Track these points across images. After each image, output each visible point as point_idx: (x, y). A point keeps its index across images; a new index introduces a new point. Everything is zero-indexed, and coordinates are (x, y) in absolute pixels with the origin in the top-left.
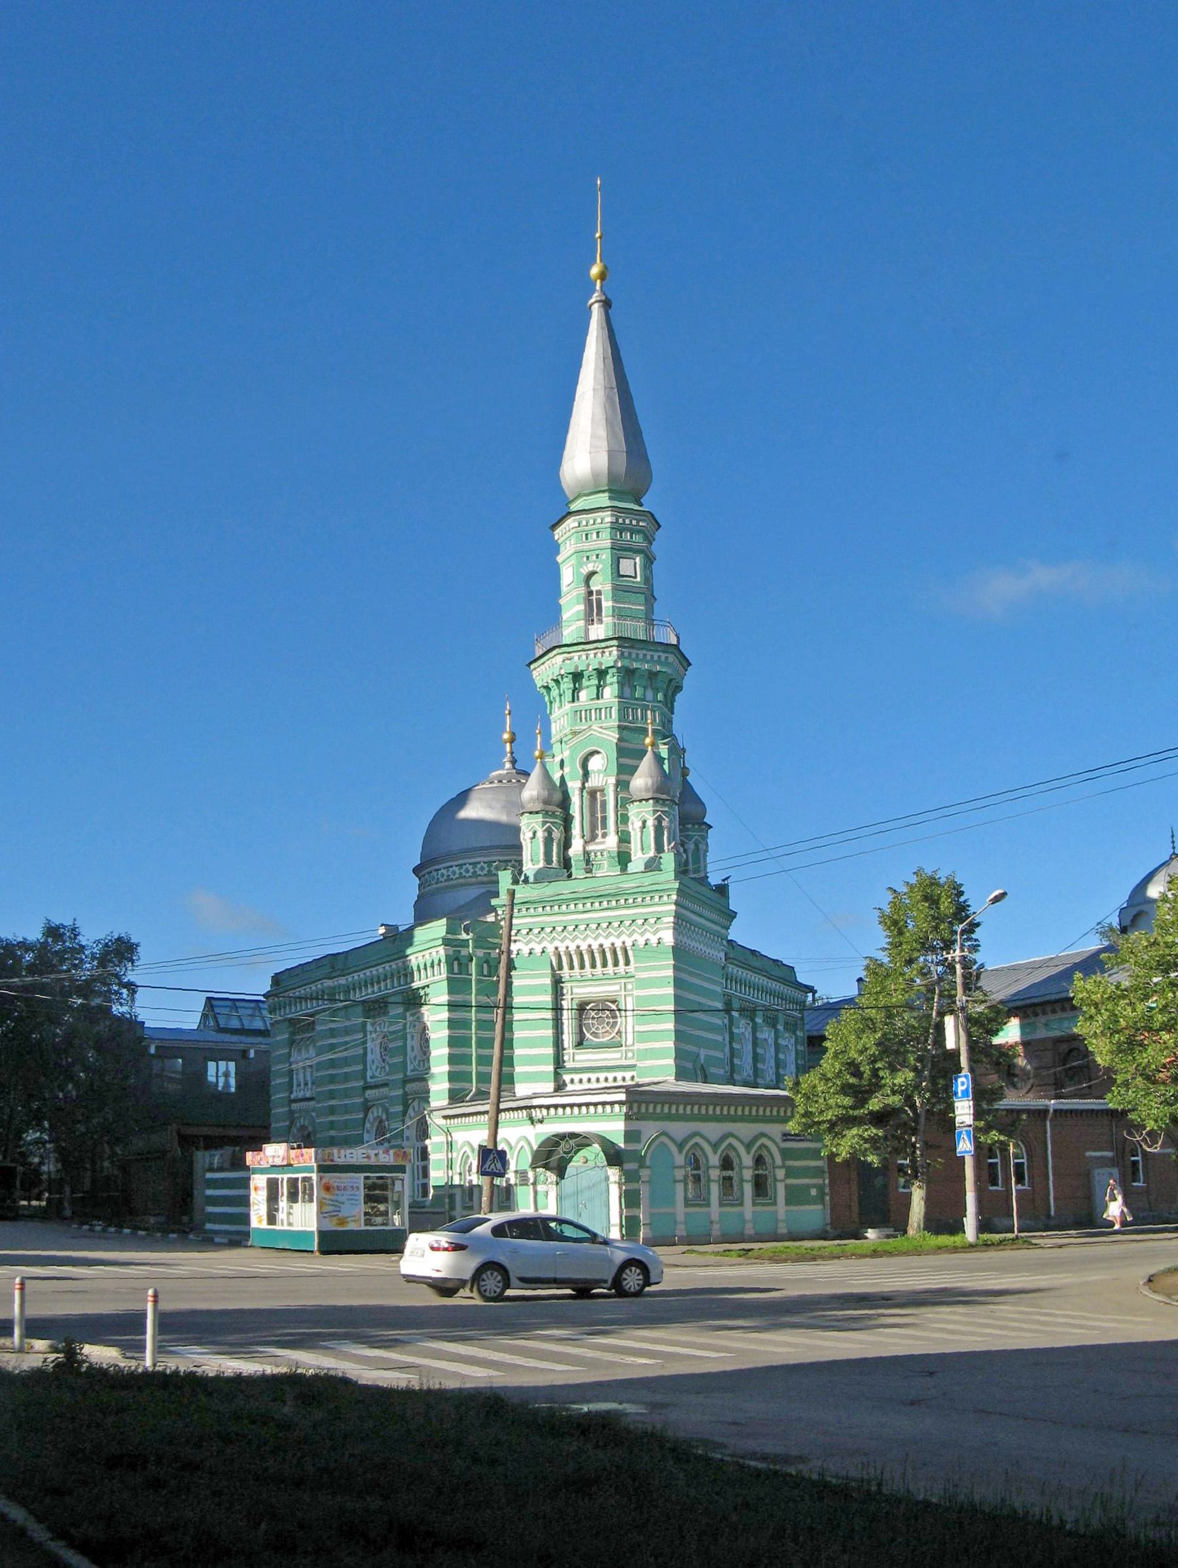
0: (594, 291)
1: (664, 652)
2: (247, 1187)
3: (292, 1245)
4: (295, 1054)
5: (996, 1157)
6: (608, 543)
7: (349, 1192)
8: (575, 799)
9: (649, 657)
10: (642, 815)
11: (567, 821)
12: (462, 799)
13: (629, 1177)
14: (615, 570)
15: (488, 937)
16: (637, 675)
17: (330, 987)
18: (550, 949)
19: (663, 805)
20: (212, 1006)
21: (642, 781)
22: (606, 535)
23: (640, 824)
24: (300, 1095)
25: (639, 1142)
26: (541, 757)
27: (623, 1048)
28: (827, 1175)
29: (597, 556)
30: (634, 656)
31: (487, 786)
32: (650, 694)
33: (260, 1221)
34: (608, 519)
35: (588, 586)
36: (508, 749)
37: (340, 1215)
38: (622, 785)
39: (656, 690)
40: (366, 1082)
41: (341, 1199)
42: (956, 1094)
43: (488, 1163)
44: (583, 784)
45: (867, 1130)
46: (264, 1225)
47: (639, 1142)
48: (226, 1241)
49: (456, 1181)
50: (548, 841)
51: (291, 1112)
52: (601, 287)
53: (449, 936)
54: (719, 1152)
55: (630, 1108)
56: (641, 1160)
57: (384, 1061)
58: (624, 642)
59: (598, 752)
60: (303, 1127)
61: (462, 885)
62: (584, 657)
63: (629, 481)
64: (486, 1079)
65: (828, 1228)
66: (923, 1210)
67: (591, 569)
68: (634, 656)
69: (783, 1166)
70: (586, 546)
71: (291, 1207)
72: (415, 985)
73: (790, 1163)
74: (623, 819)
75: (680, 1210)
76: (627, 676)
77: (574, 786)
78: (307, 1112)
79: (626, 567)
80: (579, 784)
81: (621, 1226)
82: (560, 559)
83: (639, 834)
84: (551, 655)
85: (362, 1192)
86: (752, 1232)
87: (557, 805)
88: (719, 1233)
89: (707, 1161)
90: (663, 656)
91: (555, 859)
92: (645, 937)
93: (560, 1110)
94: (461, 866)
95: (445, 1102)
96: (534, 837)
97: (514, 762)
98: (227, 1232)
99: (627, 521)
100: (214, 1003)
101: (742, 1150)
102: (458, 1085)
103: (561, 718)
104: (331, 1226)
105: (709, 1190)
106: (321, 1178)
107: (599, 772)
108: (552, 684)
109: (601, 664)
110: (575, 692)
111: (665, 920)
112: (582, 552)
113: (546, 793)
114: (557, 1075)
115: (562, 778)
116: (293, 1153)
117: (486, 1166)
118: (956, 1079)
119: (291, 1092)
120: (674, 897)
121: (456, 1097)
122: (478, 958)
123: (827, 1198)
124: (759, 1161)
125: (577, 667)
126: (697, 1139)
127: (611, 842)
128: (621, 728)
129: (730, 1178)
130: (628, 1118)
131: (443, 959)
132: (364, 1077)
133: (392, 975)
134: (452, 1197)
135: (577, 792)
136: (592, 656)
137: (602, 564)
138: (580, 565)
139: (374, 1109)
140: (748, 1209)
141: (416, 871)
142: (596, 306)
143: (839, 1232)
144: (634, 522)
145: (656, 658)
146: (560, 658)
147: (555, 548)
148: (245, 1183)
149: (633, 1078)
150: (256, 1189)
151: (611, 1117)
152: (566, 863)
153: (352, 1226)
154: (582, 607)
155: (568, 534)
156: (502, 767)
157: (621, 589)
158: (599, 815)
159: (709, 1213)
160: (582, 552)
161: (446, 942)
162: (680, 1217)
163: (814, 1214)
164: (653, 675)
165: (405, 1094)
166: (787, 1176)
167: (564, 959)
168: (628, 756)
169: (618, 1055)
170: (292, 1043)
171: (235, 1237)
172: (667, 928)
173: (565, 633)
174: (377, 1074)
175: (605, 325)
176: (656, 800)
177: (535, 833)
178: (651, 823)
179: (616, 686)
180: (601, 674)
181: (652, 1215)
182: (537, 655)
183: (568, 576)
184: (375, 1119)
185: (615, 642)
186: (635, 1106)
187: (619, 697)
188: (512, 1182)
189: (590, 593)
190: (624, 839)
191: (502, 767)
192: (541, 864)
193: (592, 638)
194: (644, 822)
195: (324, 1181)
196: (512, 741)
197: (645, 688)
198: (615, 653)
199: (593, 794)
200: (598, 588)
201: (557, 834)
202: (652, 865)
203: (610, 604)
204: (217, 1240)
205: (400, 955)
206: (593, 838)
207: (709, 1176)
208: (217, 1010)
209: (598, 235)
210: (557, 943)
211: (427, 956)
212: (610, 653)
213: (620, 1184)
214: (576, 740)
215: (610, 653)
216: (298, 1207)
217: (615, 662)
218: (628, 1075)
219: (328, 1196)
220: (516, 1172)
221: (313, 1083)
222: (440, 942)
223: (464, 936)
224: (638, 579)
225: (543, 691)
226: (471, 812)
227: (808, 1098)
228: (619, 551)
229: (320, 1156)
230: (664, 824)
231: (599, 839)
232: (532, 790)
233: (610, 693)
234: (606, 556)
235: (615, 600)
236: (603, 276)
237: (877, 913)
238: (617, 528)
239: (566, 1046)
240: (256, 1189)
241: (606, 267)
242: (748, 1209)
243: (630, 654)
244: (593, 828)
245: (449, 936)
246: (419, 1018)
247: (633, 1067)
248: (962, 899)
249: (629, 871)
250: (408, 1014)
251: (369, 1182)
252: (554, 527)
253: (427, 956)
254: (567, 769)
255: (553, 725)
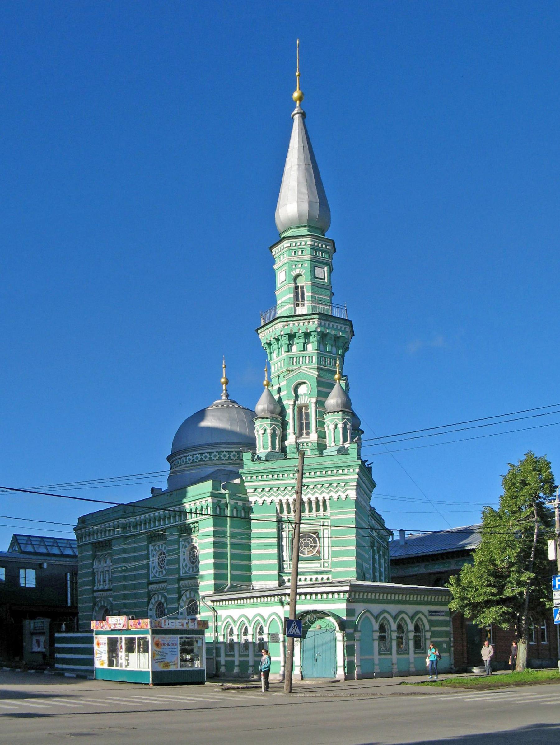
0: (295, 107)
1: (344, 324)
2: (92, 642)
3: (134, 680)
4: (96, 565)
5: (544, 626)
6: (309, 257)
7: (170, 647)
8: (289, 412)
9: (335, 327)
10: (334, 423)
11: (284, 425)
12: (201, 415)
13: (349, 637)
14: (313, 274)
15: (239, 492)
16: (328, 337)
17: (123, 523)
18: (277, 501)
19: (348, 415)
20: (17, 540)
21: (333, 400)
22: (307, 252)
23: (334, 426)
24: (101, 587)
25: (354, 616)
26: (268, 385)
27: (322, 561)
28: (452, 635)
29: (302, 265)
30: (327, 325)
31: (214, 407)
32: (334, 350)
33: (102, 664)
34: (309, 243)
35: (295, 283)
36: (224, 388)
37: (166, 661)
38: (320, 403)
39: (338, 348)
40: (149, 580)
41: (165, 651)
42: (554, 586)
43: (291, 629)
44: (295, 402)
45: (501, 608)
46: (106, 666)
47: (354, 616)
48: (74, 675)
49: (221, 639)
50: (273, 436)
51: (94, 598)
52: (300, 105)
53: (214, 491)
54: (397, 623)
55: (350, 595)
56: (355, 627)
57: (161, 568)
58: (323, 317)
59: (304, 383)
60: (102, 607)
61: (200, 465)
62: (296, 324)
63: (318, 224)
64: (235, 580)
65: (453, 666)
66: (526, 656)
67: (298, 273)
68: (327, 325)
69: (430, 631)
70: (295, 258)
71: (128, 656)
72: (189, 521)
73: (433, 629)
74: (321, 424)
75: (376, 657)
76: (323, 337)
77: (288, 403)
78: (106, 597)
79: (319, 272)
80: (292, 402)
81: (344, 667)
82: (275, 267)
83: (333, 432)
84: (274, 323)
85: (178, 647)
86: (414, 669)
87: (278, 413)
88: (397, 670)
89: (390, 627)
90: (344, 327)
91: (277, 447)
92: (338, 494)
93: (319, 596)
94: (201, 454)
95: (212, 592)
96: (265, 433)
97: (227, 396)
98: (73, 670)
99: (320, 245)
100: (18, 537)
101: (408, 620)
102: (220, 582)
103: (278, 361)
104: (160, 668)
105: (391, 645)
106: (153, 638)
107: (305, 394)
108: (273, 341)
109: (307, 329)
110: (290, 346)
111: (351, 484)
112: (290, 264)
113: (273, 407)
114: (280, 576)
115: (280, 399)
116: (131, 622)
117: (290, 630)
118: (554, 579)
119: (94, 586)
120: (357, 470)
121: (218, 589)
122: (231, 506)
123: (453, 649)
124: (417, 628)
125: (291, 330)
126: (274, 617)
127: (314, 437)
128: (319, 369)
129: (419, 636)
130: (348, 601)
131: (210, 505)
132: (179, 573)
133: (150, 520)
134: (218, 649)
135: (291, 407)
136: (301, 324)
137: (305, 270)
138: (291, 270)
139: (156, 596)
140: (394, 656)
141: (169, 459)
142: (297, 116)
143: (457, 669)
144: (324, 246)
145: (339, 328)
146: (280, 325)
147: (273, 261)
148: (90, 640)
149: (328, 579)
150: (98, 644)
151: (338, 600)
152: (283, 450)
153: (172, 668)
154: (292, 295)
155: (282, 251)
156: (220, 398)
157: (316, 285)
158: (304, 421)
159: (391, 659)
160: (290, 264)
161: (213, 495)
162: (376, 661)
163: (447, 660)
164: (337, 338)
165: (179, 587)
166: (431, 637)
167: (285, 507)
168: (324, 387)
169: (319, 565)
170: (94, 557)
171: (83, 674)
172: (351, 489)
173: (278, 312)
174: (157, 575)
175: (303, 127)
176: (344, 412)
177: (265, 430)
178: (340, 426)
179: (316, 343)
180: (307, 335)
181: (361, 660)
182: (262, 325)
183: (281, 277)
184: (156, 602)
185: (316, 316)
186: (353, 594)
187: (318, 350)
188: (266, 639)
189: (297, 287)
190: (322, 435)
191: (220, 398)
192: (269, 450)
193: (297, 314)
194: (336, 425)
195: (155, 639)
196: (227, 383)
197: (332, 346)
198: (316, 322)
199: (300, 408)
200: (302, 285)
201: (278, 432)
202: (342, 451)
203: (310, 294)
204: (67, 674)
205: (179, 503)
206: (301, 435)
207: (391, 637)
208: (20, 541)
209: (297, 74)
210: (280, 497)
211: (198, 504)
212: (313, 322)
213: (344, 642)
214: (291, 375)
215: (313, 322)
216: (134, 656)
217: (317, 328)
218: (325, 577)
219: (158, 650)
220: (269, 634)
221: (110, 580)
222: (209, 494)
223: (223, 491)
224: (326, 281)
225: (266, 346)
226: (208, 422)
227: (465, 589)
228: (315, 263)
229: (153, 624)
230: (348, 427)
231: (304, 436)
232: (261, 406)
233: (311, 348)
234: (307, 265)
235: (313, 292)
236: (300, 99)
237: (502, 478)
238: (314, 248)
239: (285, 559)
240: (98, 644)
241: (303, 94)
242: (394, 656)
243: (325, 324)
244: (301, 428)
245: (214, 491)
246: (190, 541)
247: (329, 572)
248: (550, 470)
249: (325, 454)
250: (181, 539)
251: (183, 640)
252: (272, 247)
253: (198, 504)
254: (282, 394)
255: (272, 368)
